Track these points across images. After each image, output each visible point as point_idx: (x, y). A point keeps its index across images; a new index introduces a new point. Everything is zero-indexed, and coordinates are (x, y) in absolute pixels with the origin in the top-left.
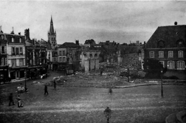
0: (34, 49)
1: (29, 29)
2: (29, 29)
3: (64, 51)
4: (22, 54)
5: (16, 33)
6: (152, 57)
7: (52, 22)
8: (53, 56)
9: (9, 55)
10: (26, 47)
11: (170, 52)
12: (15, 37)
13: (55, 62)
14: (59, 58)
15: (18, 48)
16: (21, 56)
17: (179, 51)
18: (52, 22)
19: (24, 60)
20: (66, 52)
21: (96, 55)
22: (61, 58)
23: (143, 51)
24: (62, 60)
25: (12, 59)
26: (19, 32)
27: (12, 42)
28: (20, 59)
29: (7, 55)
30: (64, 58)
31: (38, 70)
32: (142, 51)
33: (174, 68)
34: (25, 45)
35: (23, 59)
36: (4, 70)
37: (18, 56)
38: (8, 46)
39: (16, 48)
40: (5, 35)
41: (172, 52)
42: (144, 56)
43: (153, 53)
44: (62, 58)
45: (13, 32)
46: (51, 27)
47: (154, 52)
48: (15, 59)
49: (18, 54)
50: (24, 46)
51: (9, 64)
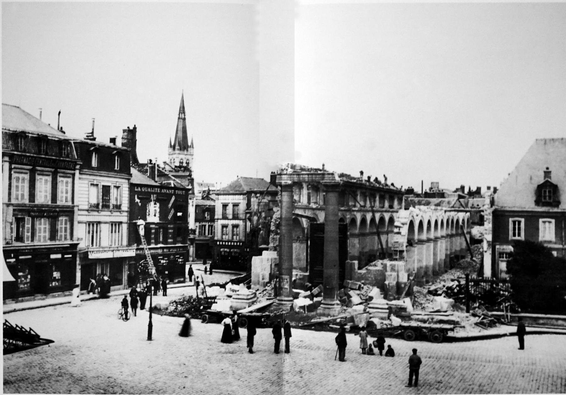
0: (153, 193)
1: (135, 128)
2: (135, 128)
3: (236, 205)
4: (118, 207)
5: (102, 139)
6: (517, 238)
7: (182, 110)
8: (196, 220)
9: (80, 207)
10: (132, 186)
11: (544, 222)
12: (101, 150)
13: (202, 238)
14: (220, 227)
15: (109, 187)
16: (115, 214)
17: (541, 220)
18: (182, 110)
19: (125, 227)
20: (242, 207)
21: (105, 202)
22: (224, 226)
23: (491, 217)
24: (230, 235)
25: (90, 223)
26: (113, 137)
27: (93, 169)
28: (113, 224)
29: (76, 209)
30: (236, 226)
31: (162, 261)
32: (485, 217)
33: (350, 255)
34: (129, 180)
35: (121, 223)
36: (63, 256)
37: (109, 213)
38: (80, 178)
39: (103, 186)
40: (72, 142)
41: (550, 222)
42: (491, 232)
43: (519, 222)
44: (230, 227)
45: (92, 133)
46: (180, 127)
47: (523, 220)
48: (99, 223)
49: (106, 206)
50: (127, 181)
51: (78, 239)
